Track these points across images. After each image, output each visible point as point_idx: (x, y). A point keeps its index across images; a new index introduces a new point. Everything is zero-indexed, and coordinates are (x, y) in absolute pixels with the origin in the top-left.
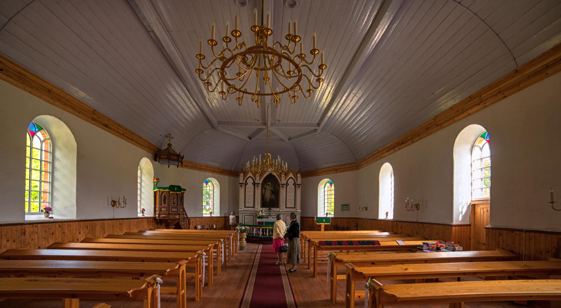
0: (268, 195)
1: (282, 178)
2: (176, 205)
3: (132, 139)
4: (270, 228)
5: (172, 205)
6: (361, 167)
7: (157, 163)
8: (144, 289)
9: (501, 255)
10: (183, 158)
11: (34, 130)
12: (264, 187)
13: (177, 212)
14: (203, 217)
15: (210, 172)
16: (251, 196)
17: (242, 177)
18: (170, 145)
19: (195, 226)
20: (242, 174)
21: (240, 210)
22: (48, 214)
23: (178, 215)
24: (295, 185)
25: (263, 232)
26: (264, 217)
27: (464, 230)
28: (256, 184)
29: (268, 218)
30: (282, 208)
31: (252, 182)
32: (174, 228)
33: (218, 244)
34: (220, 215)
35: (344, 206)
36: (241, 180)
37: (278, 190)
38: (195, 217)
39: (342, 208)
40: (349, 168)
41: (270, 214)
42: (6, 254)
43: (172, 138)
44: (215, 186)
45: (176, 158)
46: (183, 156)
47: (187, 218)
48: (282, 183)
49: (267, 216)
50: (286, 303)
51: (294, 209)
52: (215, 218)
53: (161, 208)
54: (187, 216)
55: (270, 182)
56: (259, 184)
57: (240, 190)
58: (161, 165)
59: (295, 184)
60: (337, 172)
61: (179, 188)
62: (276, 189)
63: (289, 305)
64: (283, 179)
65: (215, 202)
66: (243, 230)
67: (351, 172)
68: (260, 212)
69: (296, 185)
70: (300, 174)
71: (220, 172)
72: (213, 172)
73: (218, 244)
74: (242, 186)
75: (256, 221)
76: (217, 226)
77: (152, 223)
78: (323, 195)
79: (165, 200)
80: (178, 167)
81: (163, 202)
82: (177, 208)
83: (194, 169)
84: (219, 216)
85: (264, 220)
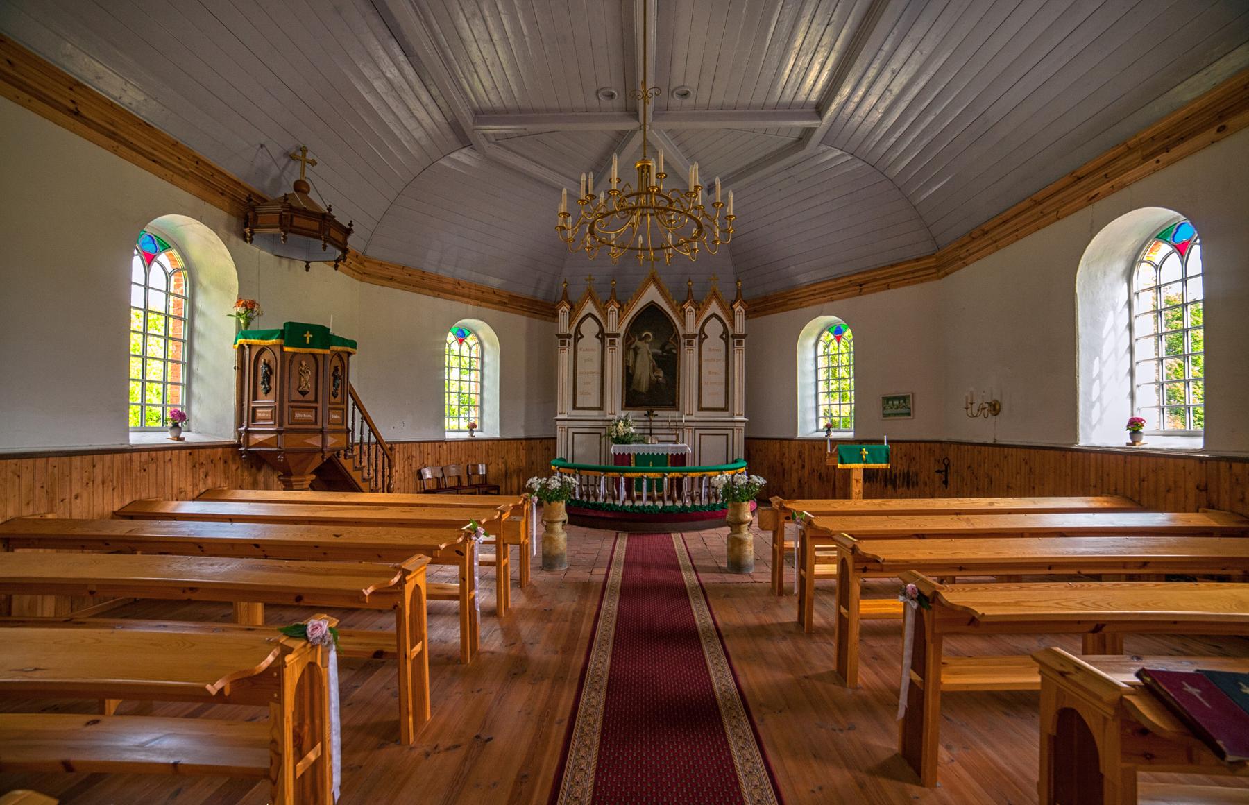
0: (645, 371)
1: (688, 317)
2: (311, 396)
4: (652, 475)
5: (293, 398)
6: (960, 263)
7: (259, 253)
8: (269, 668)
9: (1233, 525)
10: (348, 231)
11: (150, 248)
12: (633, 346)
13: (316, 423)
14: (445, 441)
15: (468, 303)
16: (591, 373)
17: (566, 317)
18: (301, 187)
19: (419, 468)
20: (565, 308)
21: (559, 417)
22: (177, 429)
23: (321, 436)
24: (728, 336)
25: (629, 489)
26: (633, 439)
27: (1096, 460)
28: (609, 335)
29: (643, 441)
30: (687, 412)
31: (596, 329)
32: (313, 487)
33: (522, 505)
34: (526, 431)
35: (890, 402)
36: (563, 325)
37: (676, 354)
38: (420, 442)
39: (884, 408)
40: (911, 276)
41: (651, 429)
42: (130, 509)
43: (313, 163)
44: (486, 345)
45: (315, 225)
46: (351, 225)
47: (379, 442)
48: (688, 331)
49: (641, 434)
50: (713, 693)
51: (726, 413)
53: (254, 409)
54: (377, 436)
55: (650, 331)
56: (617, 335)
57: (560, 355)
58: (280, 263)
59: (725, 336)
60: (863, 291)
61: (322, 336)
62: (669, 351)
63: (702, 630)
64: (690, 319)
65: (485, 395)
66: (552, 492)
67: (920, 286)
68: (621, 424)
69: (731, 339)
70: (741, 304)
71: (500, 303)
73: (522, 505)
74: (565, 345)
75: (609, 450)
76: (490, 467)
77: (220, 466)
78: (813, 368)
79: (267, 378)
81: (261, 388)
82: (316, 409)
83: (418, 289)
84: (498, 436)
85: (634, 449)
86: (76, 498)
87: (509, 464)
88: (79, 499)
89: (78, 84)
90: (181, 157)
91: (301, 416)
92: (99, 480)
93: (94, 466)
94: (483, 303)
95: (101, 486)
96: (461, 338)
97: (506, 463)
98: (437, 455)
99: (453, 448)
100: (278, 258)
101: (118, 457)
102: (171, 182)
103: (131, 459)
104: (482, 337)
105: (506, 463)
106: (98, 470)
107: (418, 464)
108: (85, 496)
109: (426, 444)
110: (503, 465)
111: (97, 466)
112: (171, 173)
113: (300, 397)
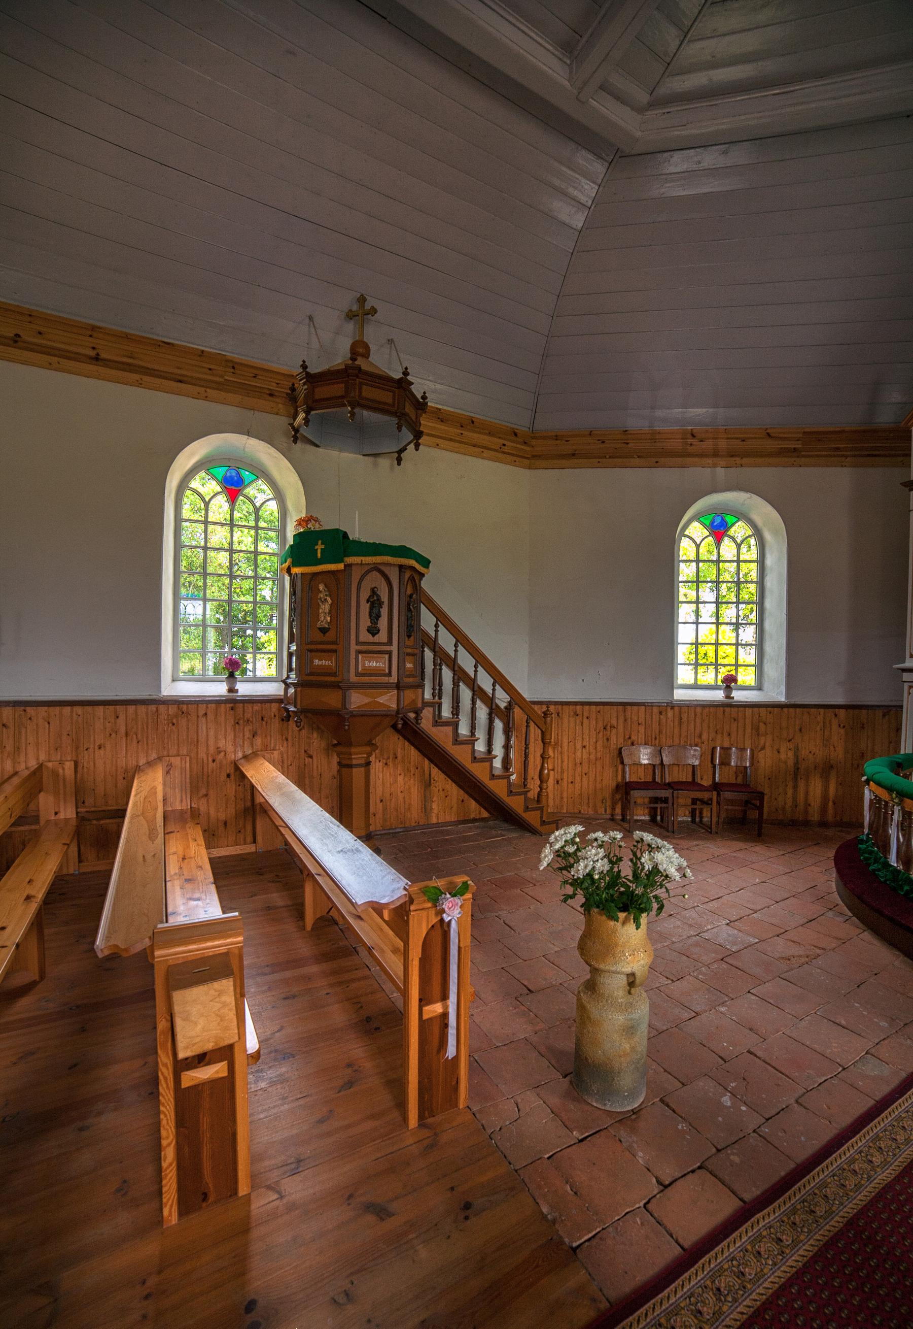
3: (91, 358)
5: (362, 639)
13: (390, 674)
14: (672, 705)
15: (715, 466)
44: (768, 536)
52: (749, 711)
58: (376, 465)
72: (738, 460)
76: (761, 755)
77: (276, 724)
80: (295, 441)
82: (390, 653)
84: (782, 699)
86: (100, 748)
87: (804, 753)
88: (103, 749)
89: (94, 328)
90: (212, 367)
91: (320, 663)
92: (123, 730)
93: (117, 717)
94: (745, 460)
95: (124, 739)
96: (719, 532)
97: (797, 750)
98: (655, 726)
99: (685, 717)
100: (371, 459)
101: (142, 709)
102: (206, 398)
103: (157, 711)
104: (759, 522)
105: (797, 750)
106: (121, 721)
107: (621, 740)
108: (108, 747)
109: (635, 708)
110: (791, 754)
111: (120, 717)
112: (203, 389)
113: (370, 638)
